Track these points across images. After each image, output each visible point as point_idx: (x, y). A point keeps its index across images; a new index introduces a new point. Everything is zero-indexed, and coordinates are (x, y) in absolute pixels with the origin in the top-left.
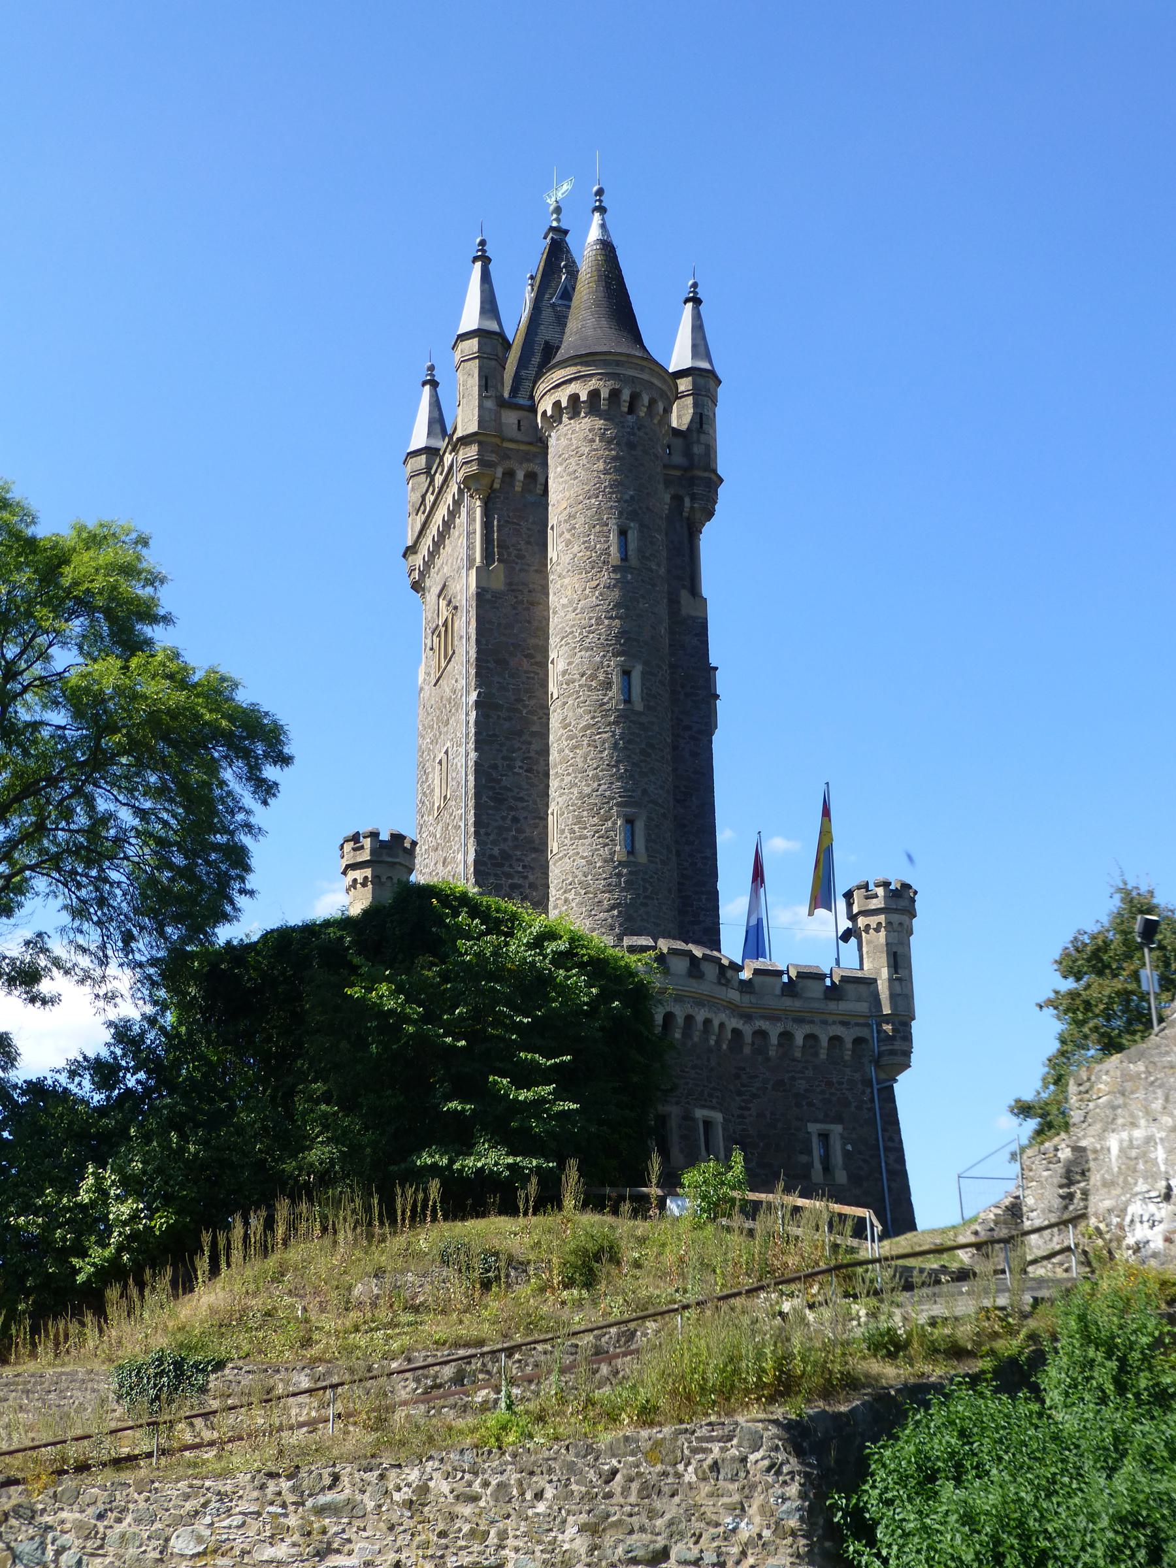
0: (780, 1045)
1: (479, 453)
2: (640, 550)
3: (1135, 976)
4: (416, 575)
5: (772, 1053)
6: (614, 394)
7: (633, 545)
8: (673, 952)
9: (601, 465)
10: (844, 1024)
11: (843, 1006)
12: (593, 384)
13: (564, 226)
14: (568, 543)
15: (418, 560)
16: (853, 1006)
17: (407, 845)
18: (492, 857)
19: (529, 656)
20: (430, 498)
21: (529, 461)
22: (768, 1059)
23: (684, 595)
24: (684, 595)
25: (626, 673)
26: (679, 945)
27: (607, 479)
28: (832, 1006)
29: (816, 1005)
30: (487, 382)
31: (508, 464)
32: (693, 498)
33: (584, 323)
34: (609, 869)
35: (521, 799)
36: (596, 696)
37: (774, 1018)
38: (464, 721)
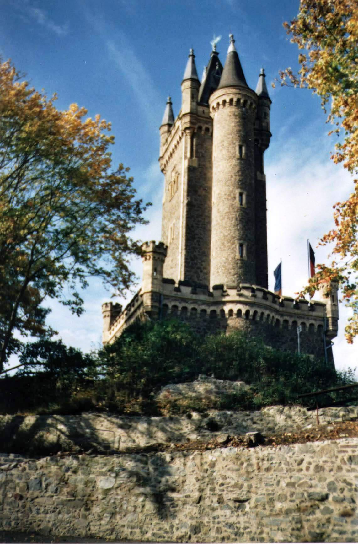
0: (292, 326)
1: (191, 120)
2: (246, 154)
3: (148, 469)
4: (163, 166)
5: (290, 328)
6: (239, 100)
7: (244, 151)
8: (258, 290)
9: (233, 124)
10: (315, 320)
11: (315, 314)
12: (231, 96)
13: (218, 51)
14: (221, 150)
15: (164, 161)
16: (318, 313)
17: (165, 247)
18: (191, 257)
19: (205, 190)
20: (170, 139)
21: (207, 124)
22: (288, 330)
23: (258, 173)
24: (258, 173)
25: (241, 195)
26: (259, 287)
27: (235, 129)
28: (311, 313)
29: (306, 313)
30: (193, 96)
31: (199, 124)
32: (262, 140)
33: (227, 76)
34: (234, 261)
35: (201, 238)
36: (231, 202)
37: (290, 315)
38: (182, 211)
